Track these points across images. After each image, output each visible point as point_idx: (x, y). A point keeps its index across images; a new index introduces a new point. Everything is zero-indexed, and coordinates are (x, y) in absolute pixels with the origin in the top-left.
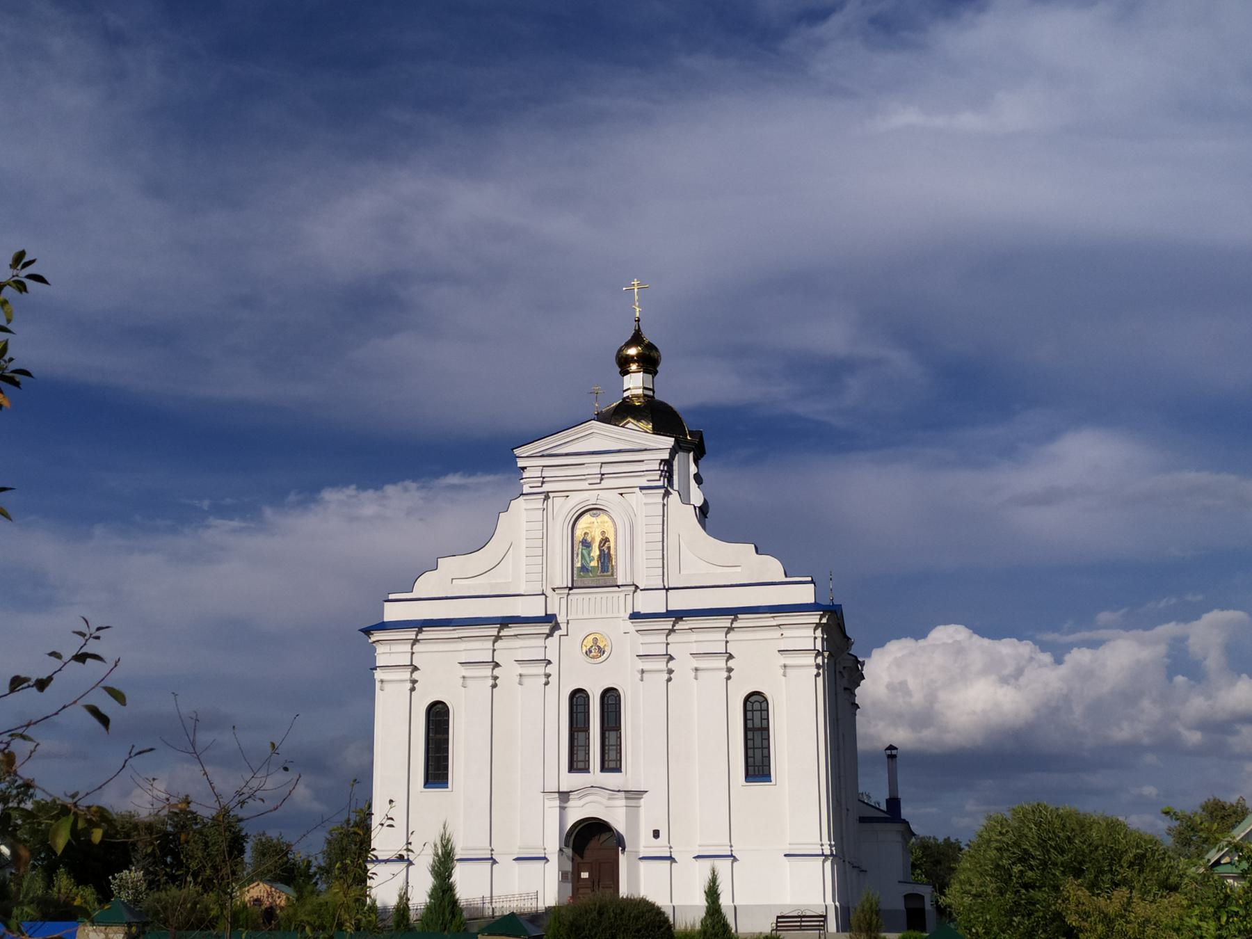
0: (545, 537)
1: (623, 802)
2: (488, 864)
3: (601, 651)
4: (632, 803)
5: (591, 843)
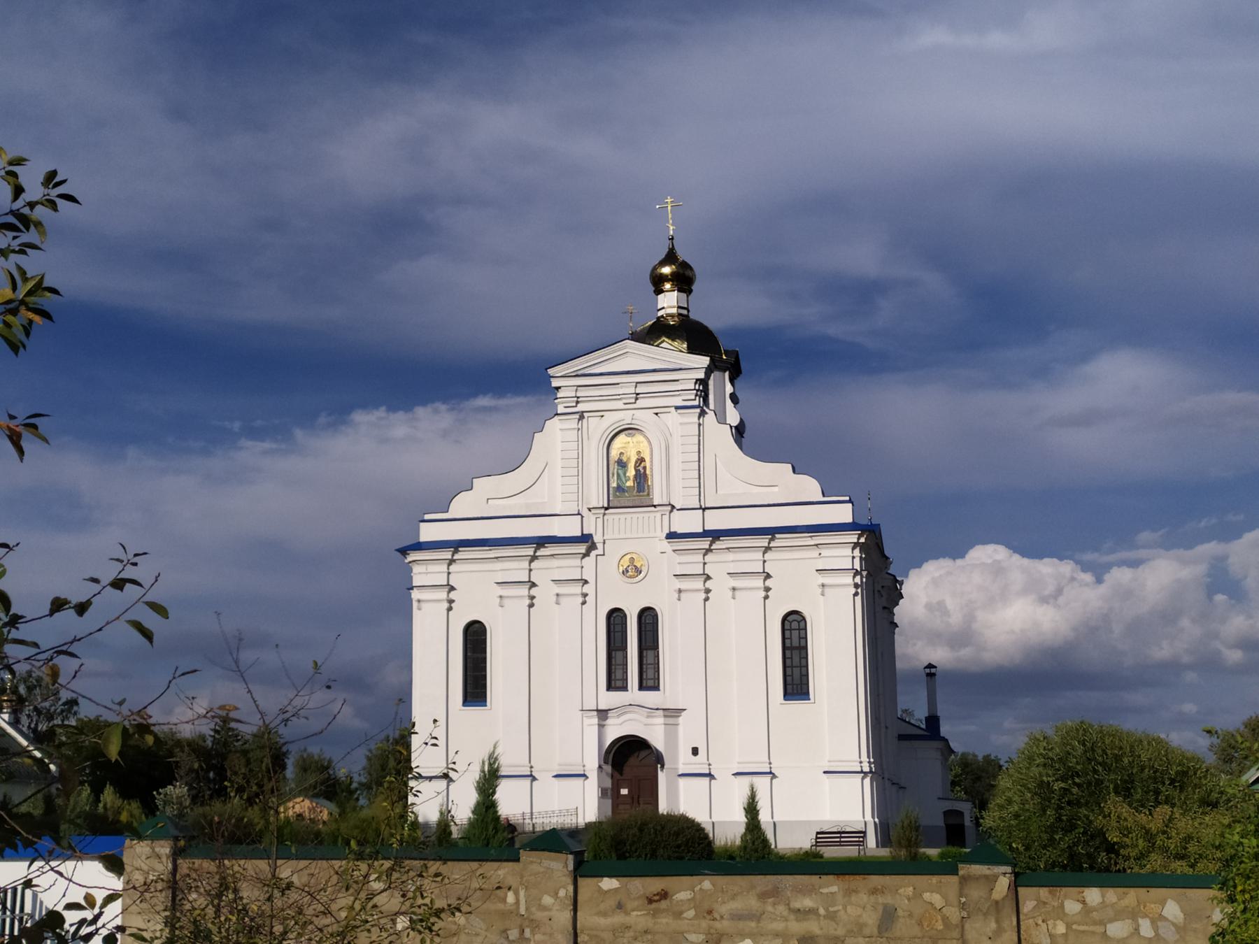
0: (580, 457)
1: (661, 720)
2: (528, 781)
4: (671, 721)
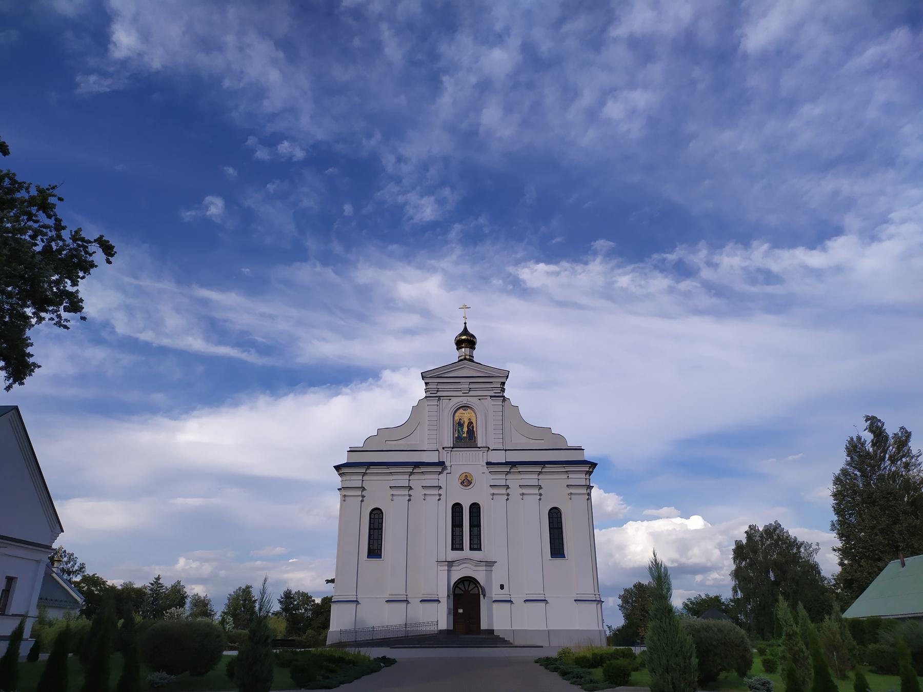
2: (404, 605)
3: (470, 483)
4: (489, 568)
5: (466, 596)
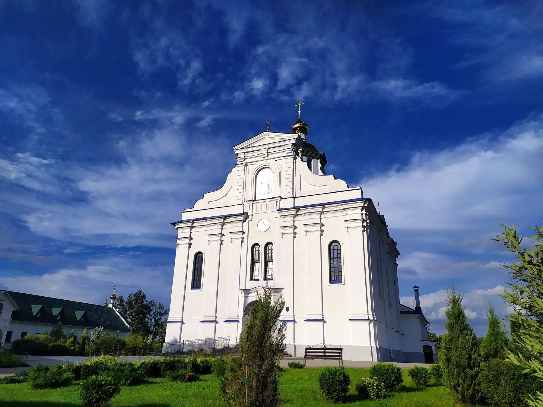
2: (214, 324)
